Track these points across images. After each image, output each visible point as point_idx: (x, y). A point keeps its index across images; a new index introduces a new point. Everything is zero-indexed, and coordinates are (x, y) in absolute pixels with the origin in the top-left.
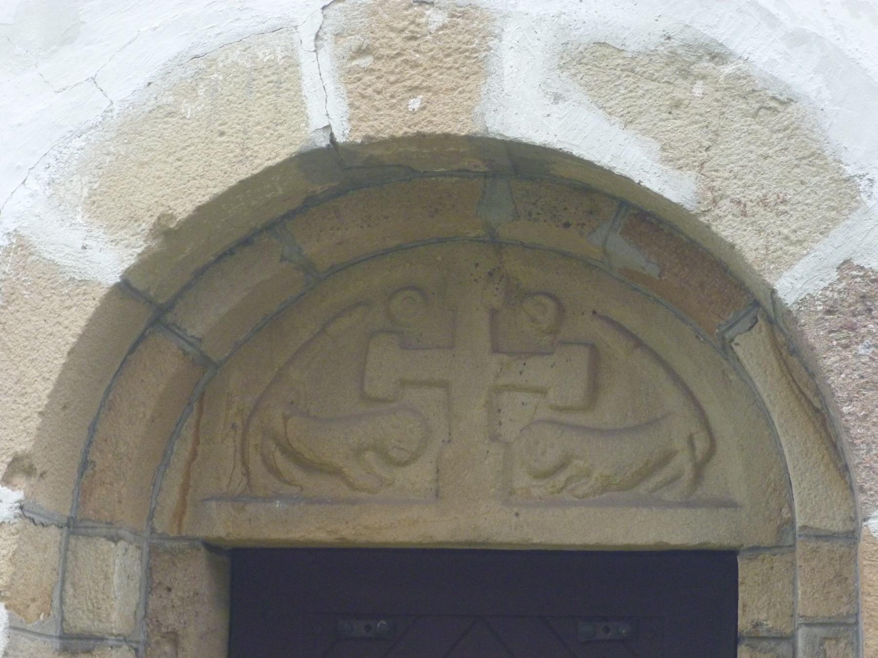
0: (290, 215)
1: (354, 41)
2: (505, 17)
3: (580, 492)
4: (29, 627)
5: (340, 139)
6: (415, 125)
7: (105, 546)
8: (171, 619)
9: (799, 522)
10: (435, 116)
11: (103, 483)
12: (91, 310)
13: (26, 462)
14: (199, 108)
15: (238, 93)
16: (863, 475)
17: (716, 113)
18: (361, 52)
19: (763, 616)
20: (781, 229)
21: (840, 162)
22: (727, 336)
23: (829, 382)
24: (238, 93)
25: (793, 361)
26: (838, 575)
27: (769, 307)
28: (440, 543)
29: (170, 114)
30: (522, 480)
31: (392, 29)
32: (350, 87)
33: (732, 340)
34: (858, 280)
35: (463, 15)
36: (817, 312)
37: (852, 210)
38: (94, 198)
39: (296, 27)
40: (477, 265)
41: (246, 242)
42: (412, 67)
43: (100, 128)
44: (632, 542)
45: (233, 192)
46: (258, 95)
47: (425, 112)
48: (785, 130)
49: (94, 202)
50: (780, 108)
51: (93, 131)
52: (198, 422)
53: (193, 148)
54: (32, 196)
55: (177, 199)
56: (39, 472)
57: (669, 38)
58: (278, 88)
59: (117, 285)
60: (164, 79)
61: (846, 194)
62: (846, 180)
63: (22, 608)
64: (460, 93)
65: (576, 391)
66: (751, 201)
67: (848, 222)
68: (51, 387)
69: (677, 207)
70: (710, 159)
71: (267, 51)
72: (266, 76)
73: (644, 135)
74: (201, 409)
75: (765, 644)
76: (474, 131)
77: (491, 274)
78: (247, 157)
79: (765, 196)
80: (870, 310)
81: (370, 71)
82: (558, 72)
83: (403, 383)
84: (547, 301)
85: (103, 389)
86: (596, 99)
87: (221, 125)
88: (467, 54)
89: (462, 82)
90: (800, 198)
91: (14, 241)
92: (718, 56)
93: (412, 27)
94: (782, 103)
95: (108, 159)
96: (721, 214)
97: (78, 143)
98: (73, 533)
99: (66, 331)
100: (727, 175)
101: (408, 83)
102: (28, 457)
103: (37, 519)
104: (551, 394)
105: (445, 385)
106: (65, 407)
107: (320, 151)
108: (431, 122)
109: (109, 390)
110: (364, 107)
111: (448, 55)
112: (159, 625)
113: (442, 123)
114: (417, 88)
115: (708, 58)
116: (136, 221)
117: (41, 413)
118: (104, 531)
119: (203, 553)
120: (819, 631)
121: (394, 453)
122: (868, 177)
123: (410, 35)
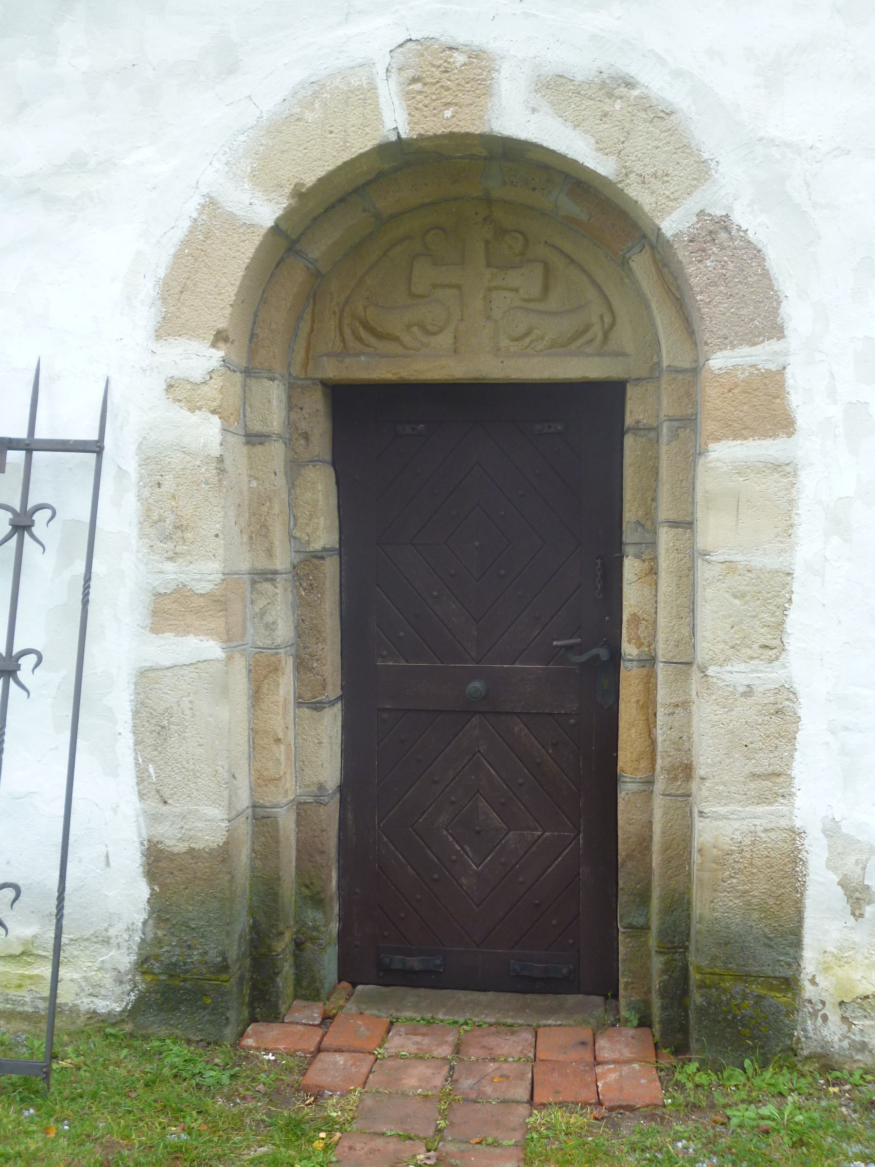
0: (368, 183)
1: (410, 73)
2: (502, 58)
3: (537, 349)
4: (231, 429)
5: (403, 136)
6: (449, 127)
7: (267, 383)
8: (303, 426)
9: (665, 363)
10: (460, 121)
11: (263, 347)
12: (257, 243)
13: (224, 334)
14: (316, 116)
15: (340, 106)
16: (707, 335)
17: (628, 120)
18: (415, 80)
19: (641, 417)
20: (665, 191)
21: (700, 151)
22: (627, 256)
23: (690, 282)
24: (340, 106)
25: (665, 270)
26: (687, 392)
27: (653, 239)
28: (458, 379)
29: (298, 120)
30: (504, 342)
31: (433, 66)
32: (409, 102)
33: (630, 258)
34: (708, 222)
35: (477, 56)
36: (684, 241)
37: (706, 180)
38: (255, 173)
39: (374, 64)
40: (477, 214)
41: (342, 200)
42: (446, 90)
43: (255, 129)
44: (568, 376)
45: (339, 169)
46: (353, 107)
47: (455, 119)
48: (669, 131)
49: (255, 176)
50: (666, 117)
51: (251, 130)
52: (313, 310)
53: (314, 141)
54: (216, 172)
55: (305, 173)
56: (231, 340)
57: (601, 73)
58: (365, 103)
59: (272, 228)
60: (293, 97)
61: (703, 170)
62: (703, 162)
63: (227, 418)
64: (475, 107)
65: (535, 290)
66: (648, 175)
67: (704, 187)
68: (236, 289)
69: (604, 178)
70: (624, 149)
71: (357, 79)
72: (357, 96)
73: (585, 133)
74: (315, 301)
75: (642, 432)
76: (484, 131)
77: (485, 219)
78: (347, 147)
79: (656, 171)
80: (714, 240)
81: (420, 92)
82: (534, 94)
83: (435, 286)
84: (518, 236)
85: (261, 291)
86: (557, 111)
87: (330, 127)
88: (479, 82)
89: (476, 100)
90: (676, 173)
91: (207, 200)
92: (630, 84)
93: (445, 64)
94: (667, 114)
95: (262, 148)
96: (630, 182)
97: (242, 138)
98: (247, 376)
99: (243, 255)
100: (634, 159)
101: (444, 100)
102: (225, 331)
103: (232, 368)
104: (521, 291)
105: (459, 287)
106: (243, 302)
107: (392, 143)
108: (458, 125)
109: (264, 291)
110: (417, 115)
111: (468, 83)
112: (297, 429)
113: (465, 126)
114: (449, 103)
115: (624, 85)
116: (281, 187)
117: (231, 305)
118: (266, 375)
119: (320, 387)
120: (676, 424)
121: (429, 327)
122: (716, 160)
123: (444, 69)
